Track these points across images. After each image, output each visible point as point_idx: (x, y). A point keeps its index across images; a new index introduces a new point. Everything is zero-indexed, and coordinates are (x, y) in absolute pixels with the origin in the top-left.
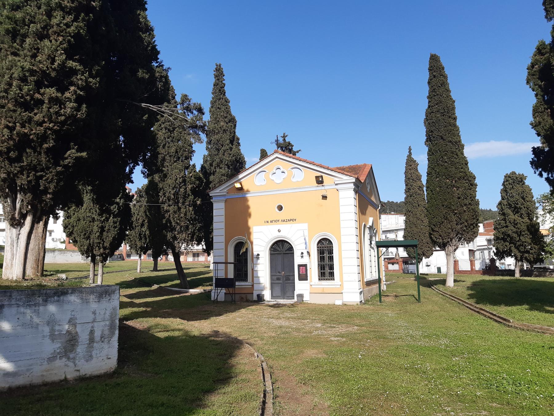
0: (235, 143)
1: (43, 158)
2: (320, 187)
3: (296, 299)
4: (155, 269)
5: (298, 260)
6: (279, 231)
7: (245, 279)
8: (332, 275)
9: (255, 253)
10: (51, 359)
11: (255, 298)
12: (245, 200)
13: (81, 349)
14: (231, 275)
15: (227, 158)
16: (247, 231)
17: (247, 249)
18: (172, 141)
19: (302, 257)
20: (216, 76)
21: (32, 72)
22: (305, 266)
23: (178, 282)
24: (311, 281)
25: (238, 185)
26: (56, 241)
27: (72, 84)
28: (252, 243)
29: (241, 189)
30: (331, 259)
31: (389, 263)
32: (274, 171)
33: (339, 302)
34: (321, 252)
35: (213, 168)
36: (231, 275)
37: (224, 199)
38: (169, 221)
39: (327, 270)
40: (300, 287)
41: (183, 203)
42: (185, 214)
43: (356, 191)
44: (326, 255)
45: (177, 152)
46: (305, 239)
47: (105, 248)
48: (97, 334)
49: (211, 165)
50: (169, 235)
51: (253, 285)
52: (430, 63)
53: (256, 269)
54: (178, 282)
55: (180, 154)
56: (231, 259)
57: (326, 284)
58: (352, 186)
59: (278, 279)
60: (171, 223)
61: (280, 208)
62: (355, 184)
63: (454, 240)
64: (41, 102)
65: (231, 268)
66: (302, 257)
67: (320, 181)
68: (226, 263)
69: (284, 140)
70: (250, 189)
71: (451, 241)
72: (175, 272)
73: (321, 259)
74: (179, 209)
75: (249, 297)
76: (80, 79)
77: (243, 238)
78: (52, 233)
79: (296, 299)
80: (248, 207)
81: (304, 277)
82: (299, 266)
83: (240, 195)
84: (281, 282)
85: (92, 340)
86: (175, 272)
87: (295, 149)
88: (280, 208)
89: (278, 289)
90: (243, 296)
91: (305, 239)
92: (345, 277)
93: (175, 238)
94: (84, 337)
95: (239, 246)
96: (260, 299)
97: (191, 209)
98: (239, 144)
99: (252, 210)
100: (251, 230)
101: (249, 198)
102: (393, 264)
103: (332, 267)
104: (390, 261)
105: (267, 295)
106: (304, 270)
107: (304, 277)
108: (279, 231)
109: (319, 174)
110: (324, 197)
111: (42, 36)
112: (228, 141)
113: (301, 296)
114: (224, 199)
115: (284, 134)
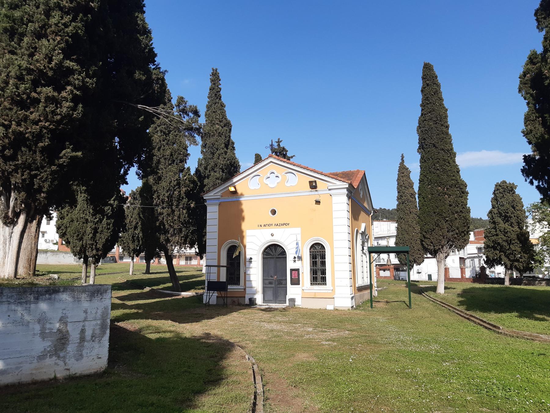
0: (229, 147)
1: (38, 157)
2: (314, 192)
3: (287, 304)
4: (148, 272)
5: (290, 265)
6: (272, 235)
7: (237, 282)
8: (324, 279)
9: (248, 257)
10: (41, 357)
11: (247, 301)
12: (239, 203)
13: (71, 348)
14: (223, 279)
15: (221, 162)
16: (240, 235)
17: (240, 252)
18: (167, 144)
19: (295, 261)
20: (212, 81)
21: (29, 71)
22: (298, 270)
23: (170, 285)
24: (303, 286)
25: (232, 189)
26: (49, 242)
27: (69, 83)
28: (245, 247)
29: (235, 192)
30: (323, 263)
31: (380, 270)
32: (268, 175)
33: (330, 307)
34: (313, 257)
35: (207, 172)
36: (223, 279)
37: (218, 202)
38: (162, 223)
39: (319, 275)
40: (292, 291)
41: (177, 206)
42: (179, 217)
43: (349, 197)
44: (319, 260)
45: (171, 155)
46: (297, 244)
47: (97, 250)
48: (88, 333)
49: (206, 168)
50: (162, 238)
51: (245, 289)
52: (424, 71)
53: (248, 273)
54: (170, 285)
55: (175, 157)
56: (224, 262)
57: (318, 289)
58: (345, 191)
59: (270, 283)
60: (164, 225)
61: (274, 212)
62: (348, 189)
63: (445, 247)
64: (38, 101)
65: (223, 271)
66: (295, 261)
67: (313, 186)
68: (219, 266)
69: (279, 145)
70: (244, 193)
71: (442, 248)
72: (168, 275)
73: (314, 263)
74: (173, 211)
75: (241, 301)
76: (77, 79)
77: (237, 242)
78: (45, 235)
79: (287, 304)
80: (242, 211)
81: (296, 282)
82: (292, 270)
83: (234, 199)
84: (273, 286)
85: (82, 339)
86: (168, 275)
87: (289, 154)
88: (274, 212)
89: (270, 293)
90: (235, 299)
91: (297, 244)
92: (337, 282)
93: (168, 241)
94: (74, 336)
95: (232, 249)
96: (252, 303)
97: (185, 211)
98: (234, 148)
99: (246, 214)
100: (244, 234)
101: (243, 202)
102: (384, 271)
103: (324, 272)
104: (381, 268)
105: (259, 299)
106: (296, 275)
107: (296, 282)
108: (272, 235)
109: (313, 179)
110: (318, 202)
111: (40, 35)
112: (223, 145)
113: (292, 300)
114: (218, 202)
115: (279, 139)
